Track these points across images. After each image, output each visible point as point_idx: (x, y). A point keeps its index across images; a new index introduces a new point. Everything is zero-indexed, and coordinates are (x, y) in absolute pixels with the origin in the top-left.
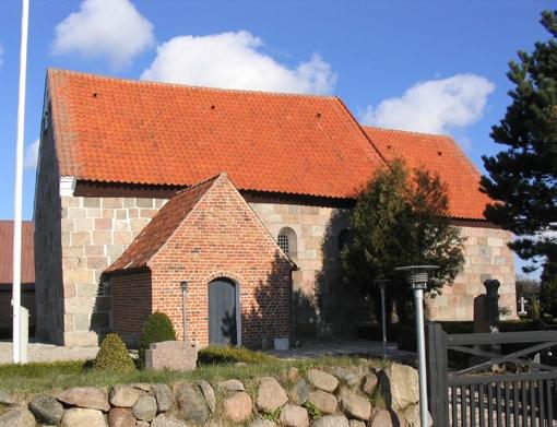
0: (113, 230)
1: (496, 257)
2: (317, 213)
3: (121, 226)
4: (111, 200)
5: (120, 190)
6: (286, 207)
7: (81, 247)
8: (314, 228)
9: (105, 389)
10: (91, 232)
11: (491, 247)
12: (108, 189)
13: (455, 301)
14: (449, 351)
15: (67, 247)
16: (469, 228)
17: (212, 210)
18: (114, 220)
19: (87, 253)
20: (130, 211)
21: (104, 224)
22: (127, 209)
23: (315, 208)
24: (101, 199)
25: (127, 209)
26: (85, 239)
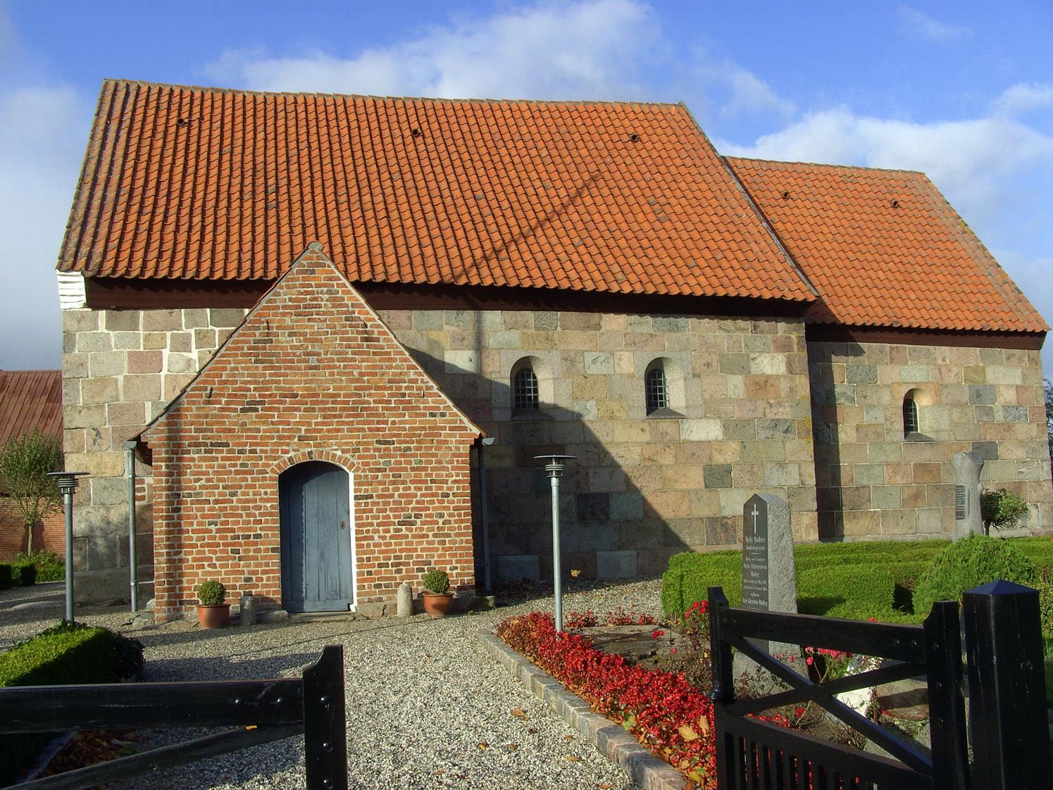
0: (164, 372)
1: (1006, 408)
2: (598, 327)
3: (181, 365)
4: (159, 315)
5: (883, 334)
6: (529, 316)
7: (100, 407)
8: (589, 357)
9: (855, 530)
10: (121, 378)
11: (993, 387)
12: (878, 334)
13: (916, 497)
14: (897, 586)
15: (74, 407)
16: (946, 349)
17: (288, 320)
18: (166, 353)
19: (113, 419)
20: (198, 333)
21: (146, 362)
22: (192, 331)
23: (594, 317)
24: (142, 313)
25: (185, 330)
26: (110, 391)
